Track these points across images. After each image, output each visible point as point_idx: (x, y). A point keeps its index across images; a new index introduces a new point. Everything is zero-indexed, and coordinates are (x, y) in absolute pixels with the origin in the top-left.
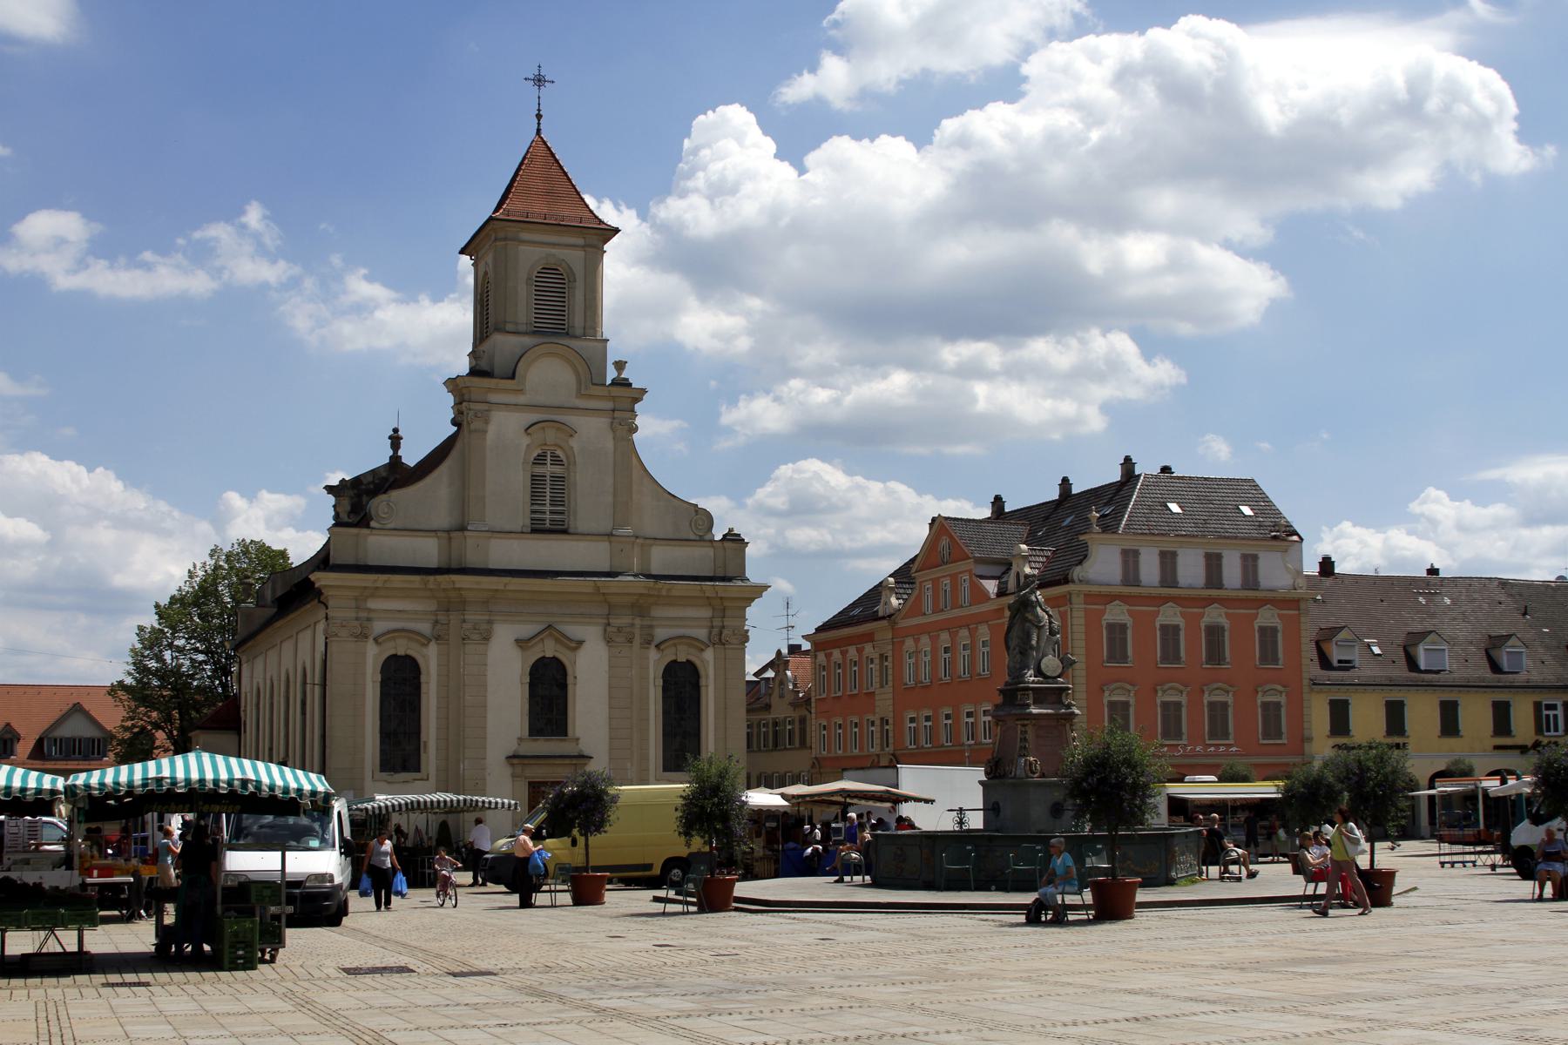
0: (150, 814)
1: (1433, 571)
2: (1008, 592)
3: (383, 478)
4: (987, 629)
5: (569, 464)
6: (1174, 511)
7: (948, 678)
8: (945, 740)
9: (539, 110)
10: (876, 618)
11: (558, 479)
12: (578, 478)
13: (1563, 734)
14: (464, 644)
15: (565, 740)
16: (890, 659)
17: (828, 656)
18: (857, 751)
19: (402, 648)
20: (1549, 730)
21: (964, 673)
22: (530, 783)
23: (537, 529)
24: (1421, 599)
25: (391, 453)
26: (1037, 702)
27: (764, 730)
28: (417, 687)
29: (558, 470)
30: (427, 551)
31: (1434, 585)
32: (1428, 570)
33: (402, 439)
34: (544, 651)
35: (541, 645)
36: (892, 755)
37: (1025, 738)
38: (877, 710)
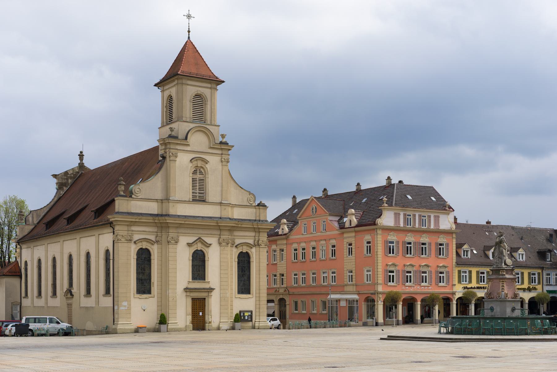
1: (488, 223)
2: (345, 227)
3: (77, 172)
5: (205, 174)
6: (410, 198)
8: (294, 283)
9: (189, 29)
11: (201, 180)
13: (537, 284)
14: (169, 244)
15: (205, 282)
16: (285, 251)
19: (145, 245)
20: (481, 282)
22: (192, 298)
24: (487, 233)
25: (79, 161)
26: (507, 273)
28: (249, 263)
29: (201, 177)
30: (153, 208)
31: (490, 228)
32: (486, 222)
33: (84, 156)
34: (197, 247)
35: (196, 245)
38: (278, 270)
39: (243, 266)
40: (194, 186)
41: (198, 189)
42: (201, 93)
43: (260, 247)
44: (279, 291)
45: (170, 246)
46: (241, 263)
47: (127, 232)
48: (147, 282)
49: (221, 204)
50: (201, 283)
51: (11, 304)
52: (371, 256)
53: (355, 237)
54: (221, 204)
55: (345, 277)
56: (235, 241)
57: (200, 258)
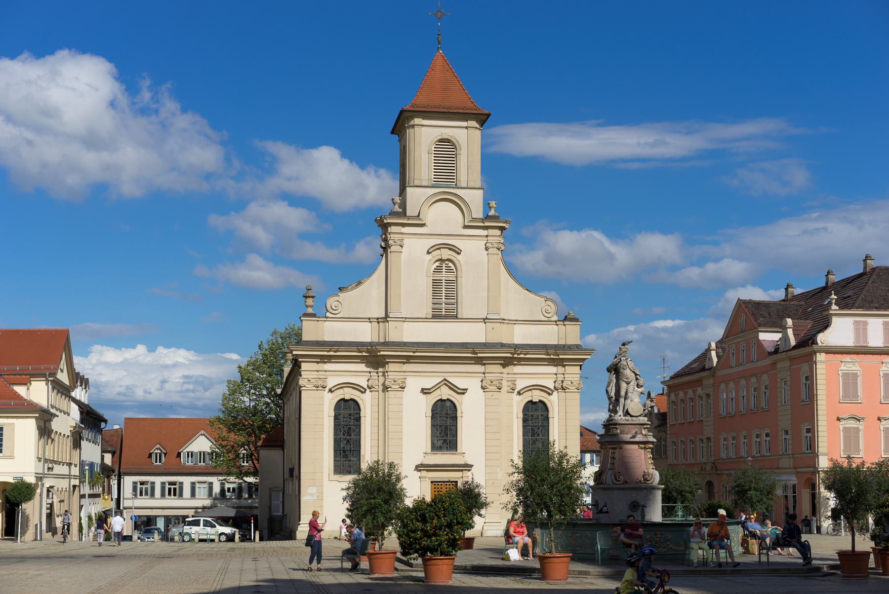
0: (796, 479)
4: (733, 384)
7: (767, 407)
10: (703, 369)
12: (463, 281)
15: (455, 454)
17: (677, 395)
18: (694, 460)
21: (755, 408)
23: (437, 316)
27: (664, 443)
30: (365, 333)
36: (713, 463)
37: (613, 463)
39: (536, 426)
40: (436, 293)
41: (444, 297)
42: (449, 138)
43: (565, 392)
44: (705, 468)
45: (390, 394)
46: (531, 420)
47: (316, 373)
48: (353, 455)
49: (485, 320)
50: (448, 455)
51: (269, 490)
52: (809, 402)
53: (790, 369)
54: (486, 321)
55: (780, 443)
56: (516, 383)
57: (447, 414)
